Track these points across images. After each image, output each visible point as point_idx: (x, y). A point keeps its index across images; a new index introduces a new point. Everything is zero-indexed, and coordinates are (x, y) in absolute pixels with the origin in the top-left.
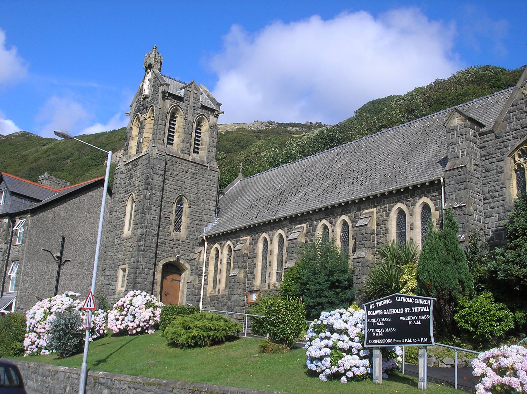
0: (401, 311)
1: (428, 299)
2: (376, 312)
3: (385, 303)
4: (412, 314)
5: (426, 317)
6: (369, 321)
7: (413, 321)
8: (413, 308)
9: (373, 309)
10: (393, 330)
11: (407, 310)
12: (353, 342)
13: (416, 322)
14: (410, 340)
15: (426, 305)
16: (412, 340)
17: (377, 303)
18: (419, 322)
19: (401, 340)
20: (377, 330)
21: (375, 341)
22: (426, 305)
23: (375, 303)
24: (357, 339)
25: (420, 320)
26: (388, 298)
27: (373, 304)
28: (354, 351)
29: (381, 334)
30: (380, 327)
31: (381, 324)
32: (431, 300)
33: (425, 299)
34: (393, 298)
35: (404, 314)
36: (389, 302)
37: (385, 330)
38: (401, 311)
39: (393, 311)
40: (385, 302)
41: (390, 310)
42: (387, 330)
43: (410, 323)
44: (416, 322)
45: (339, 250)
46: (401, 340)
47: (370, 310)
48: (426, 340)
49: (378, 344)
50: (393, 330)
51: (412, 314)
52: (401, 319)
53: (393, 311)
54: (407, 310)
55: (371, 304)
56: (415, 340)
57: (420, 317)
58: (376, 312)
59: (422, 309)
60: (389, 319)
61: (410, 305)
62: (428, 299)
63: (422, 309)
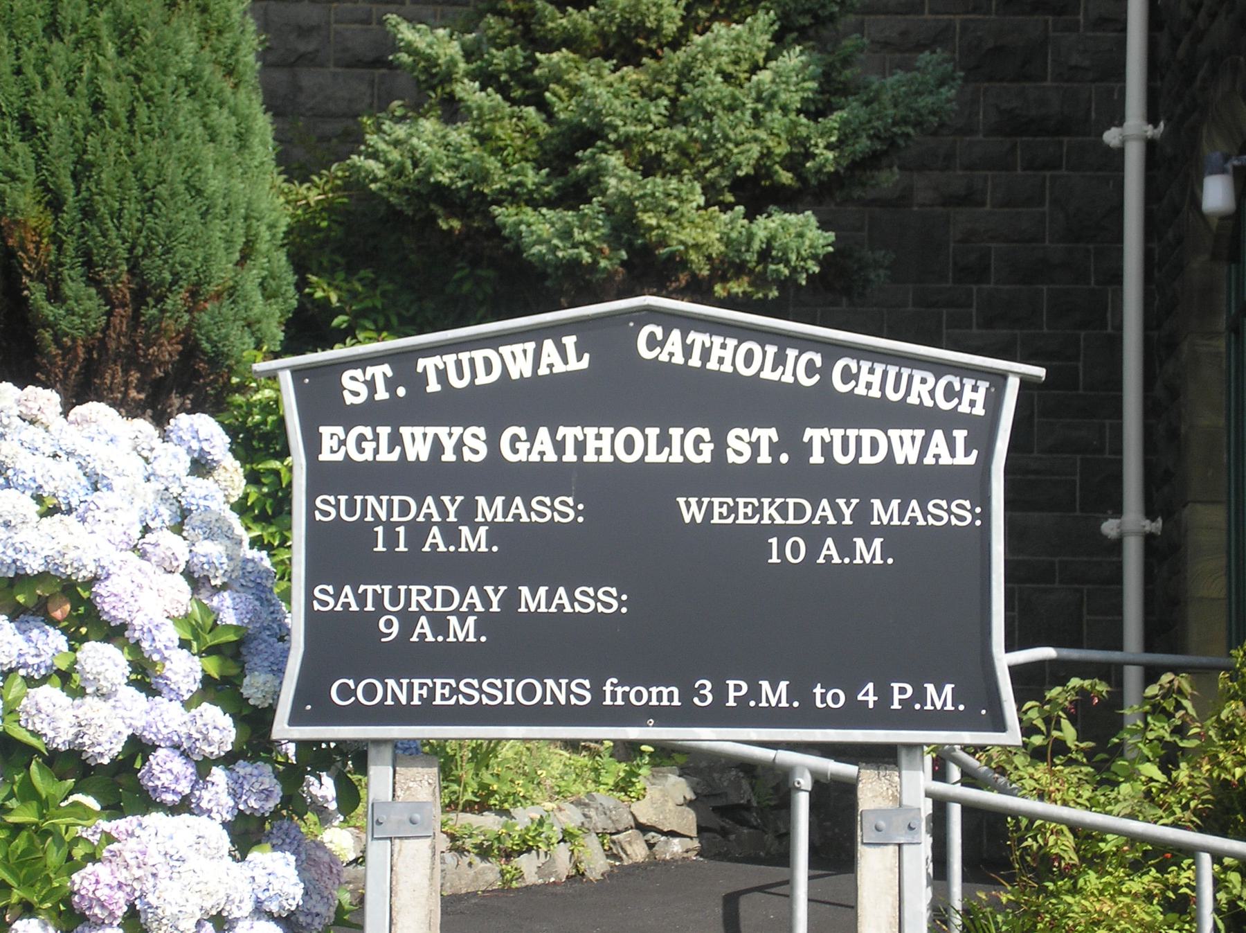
0: (689, 446)
1: (964, 371)
2: (417, 443)
3: (521, 368)
4: (795, 476)
5: (956, 513)
6: (332, 507)
7: (814, 535)
8: (815, 435)
9: (371, 413)
10: (603, 600)
11: (748, 444)
12: (79, 693)
13: (846, 548)
14: (775, 694)
15: (949, 421)
16: (800, 691)
17: (427, 364)
18: (869, 552)
19: (688, 693)
20: (418, 596)
21: (394, 690)
22: (949, 421)
23: (403, 361)
24: (185, 670)
25: (883, 530)
26: (555, 331)
27: (381, 372)
28: (168, 772)
29: (463, 631)
30: (463, 570)
31: (474, 541)
32: (1003, 376)
33: (939, 367)
34: (608, 340)
35: (718, 477)
36: (564, 359)
37: (511, 599)
38: (689, 446)
39: (603, 444)
40: (518, 361)
41: (569, 433)
42: (532, 600)
43: (795, 552)
44: (846, 548)
45: (393, 18)
46: (688, 693)
47: (349, 417)
48: (940, 697)
49: (427, 713)
50: (603, 600)
51: (795, 476)
52: (691, 510)
53: (603, 444)
54: (748, 444)
55: (362, 362)
56: (826, 697)
57: (884, 513)
58: (417, 443)
59: (904, 446)
60: (561, 510)
61: (790, 409)
62: (964, 371)
63: (904, 446)
